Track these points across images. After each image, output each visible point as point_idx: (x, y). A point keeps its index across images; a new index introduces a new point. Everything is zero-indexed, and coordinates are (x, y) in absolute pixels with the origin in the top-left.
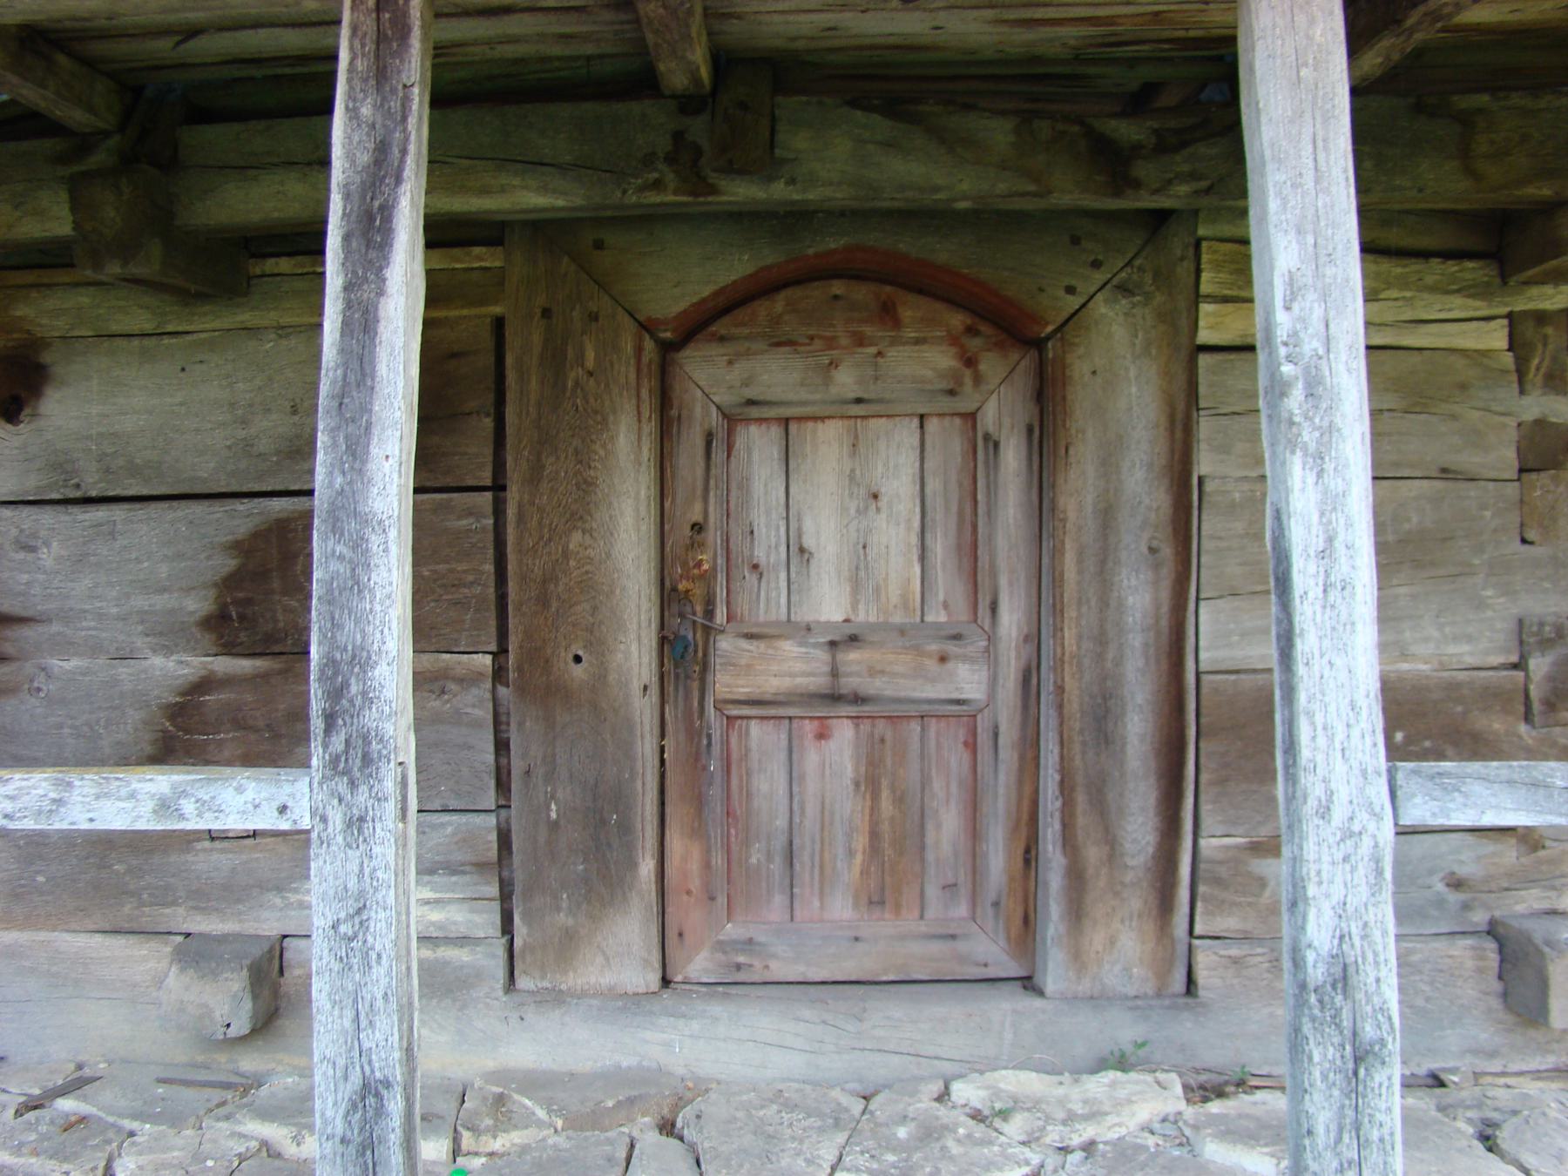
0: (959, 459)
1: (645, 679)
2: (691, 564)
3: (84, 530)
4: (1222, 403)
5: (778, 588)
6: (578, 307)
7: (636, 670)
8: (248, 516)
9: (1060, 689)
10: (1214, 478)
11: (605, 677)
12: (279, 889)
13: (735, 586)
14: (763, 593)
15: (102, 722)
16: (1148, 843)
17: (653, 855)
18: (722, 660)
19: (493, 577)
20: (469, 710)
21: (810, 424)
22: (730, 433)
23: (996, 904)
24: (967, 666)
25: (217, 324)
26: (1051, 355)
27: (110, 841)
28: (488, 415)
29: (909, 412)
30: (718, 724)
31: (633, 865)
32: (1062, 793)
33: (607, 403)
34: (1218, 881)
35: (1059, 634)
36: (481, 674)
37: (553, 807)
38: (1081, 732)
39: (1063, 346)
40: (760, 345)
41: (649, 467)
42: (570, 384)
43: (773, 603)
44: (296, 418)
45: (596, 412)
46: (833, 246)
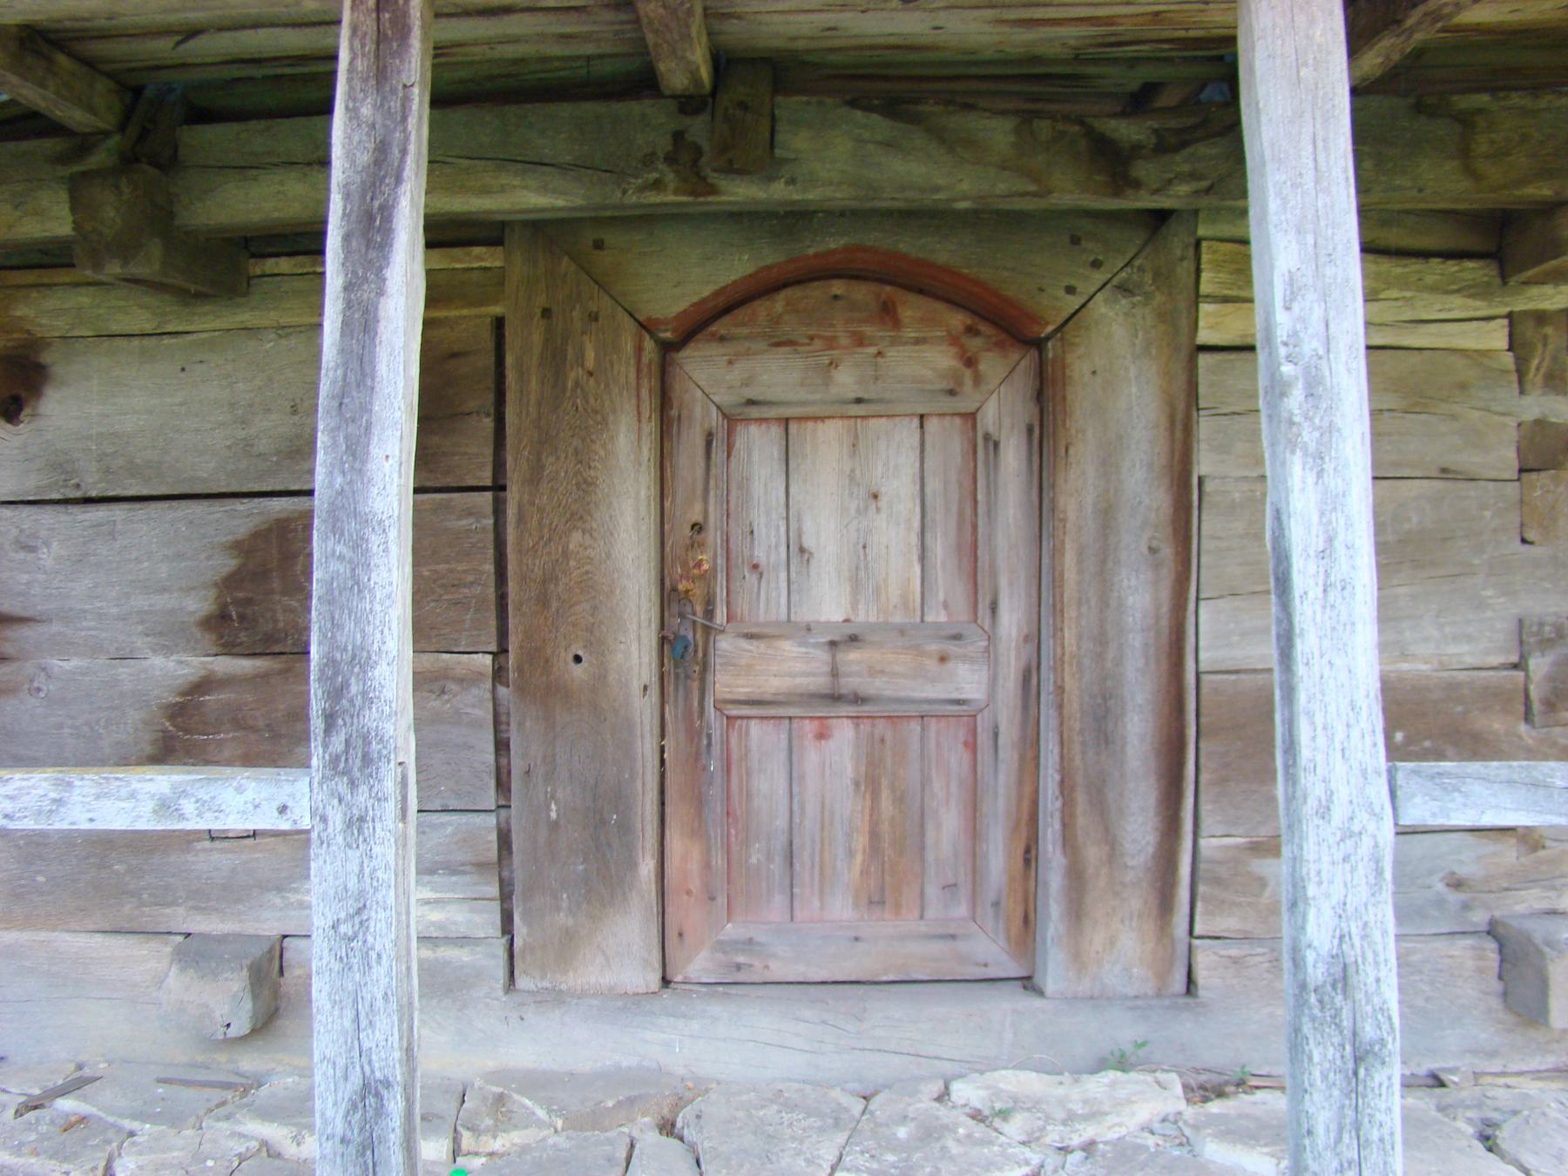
0: (959, 459)
1: (645, 679)
2: (691, 564)
4: (1222, 403)
5: (777, 588)
6: (578, 307)
8: (248, 516)
9: (1060, 689)
10: (1215, 478)
11: (605, 677)
12: (279, 889)
13: (735, 585)
15: (102, 723)
16: (1148, 843)
19: (493, 577)
20: (469, 710)
21: (810, 424)
22: (730, 432)
23: (996, 904)
24: (967, 666)
25: (217, 324)
26: (1050, 355)
28: (488, 415)
29: (909, 412)
31: (632, 865)
32: (1062, 793)
33: (607, 403)
34: (1217, 881)
35: (1059, 634)
36: (481, 674)
37: (553, 807)
38: (1081, 732)
39: (1063, 346)
40: (762, 345)
41: (649, 467)
42: (570, 384)
44: (296, 418)
45: (596, 412)
46: (832, 246)
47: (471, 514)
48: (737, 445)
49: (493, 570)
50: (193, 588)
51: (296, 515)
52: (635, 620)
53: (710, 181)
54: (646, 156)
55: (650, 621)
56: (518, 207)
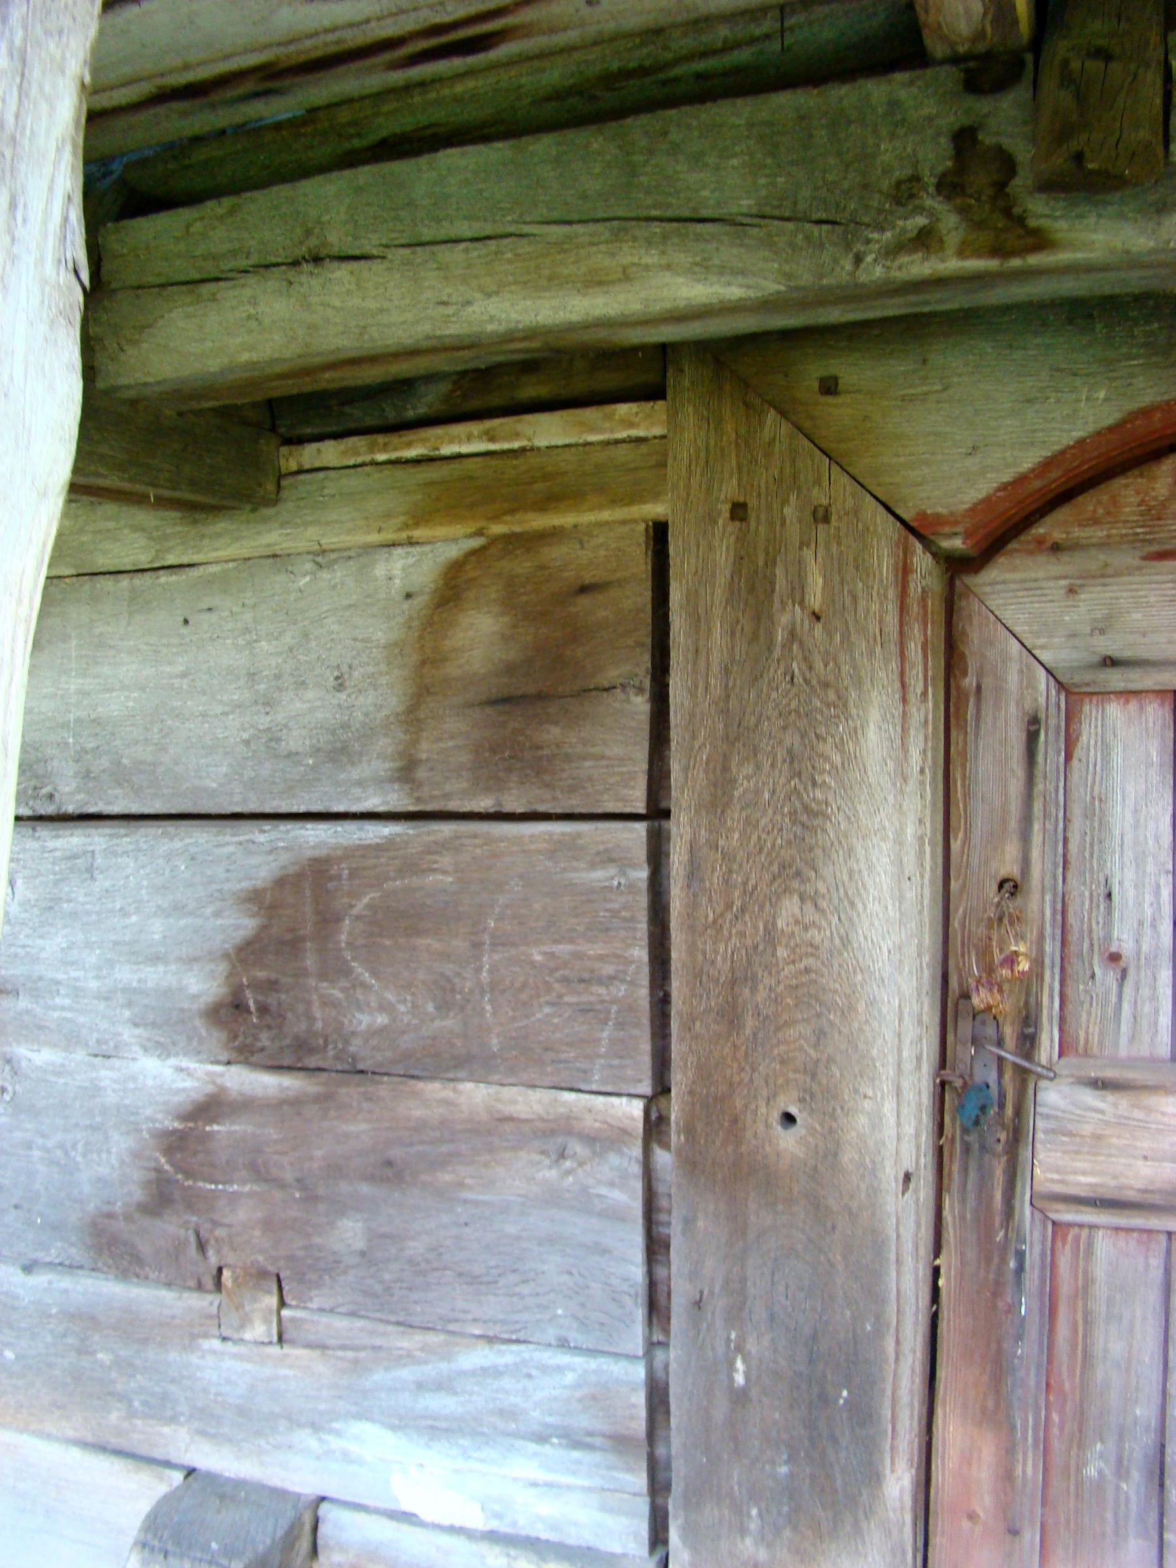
1: (908, 1164)
2: (998, 957)
3: (54, 863)
5: (1154, 998)
6: (793, 498)
7: (891, 1146)
8: (270, 852)
11: (835, 1155)
12: (316, 1427)
13: (1078, 989)
14: (1126, 1006)
15: (80, 1147)
17: (911, 1460)
18: (1052, 1124)
19: (646, 970)
20: (604, 1191)
22: (1071, 717)
25: (233, 551)
27: (93, 1318)
28: (640, 690)
30: (1037, 1235)
31: (875, 1478)
33: (846, 668)
36: (624, 1131)
37: (739, 1365)
40: (1127, 558)
41: (922, 783)
42: (780, 636)
43: (1144, 1023)
44: (343, 696)
45: (826, 685)
47: (612, 860)
48: (1084, 738)
49: (646, 958)
50: (196, 959)
51: (339, 853)
52: (891, 1059)
53: (1032, 223)
54: (899, 183)
55: (919, 1059)
56: (657, 308)
